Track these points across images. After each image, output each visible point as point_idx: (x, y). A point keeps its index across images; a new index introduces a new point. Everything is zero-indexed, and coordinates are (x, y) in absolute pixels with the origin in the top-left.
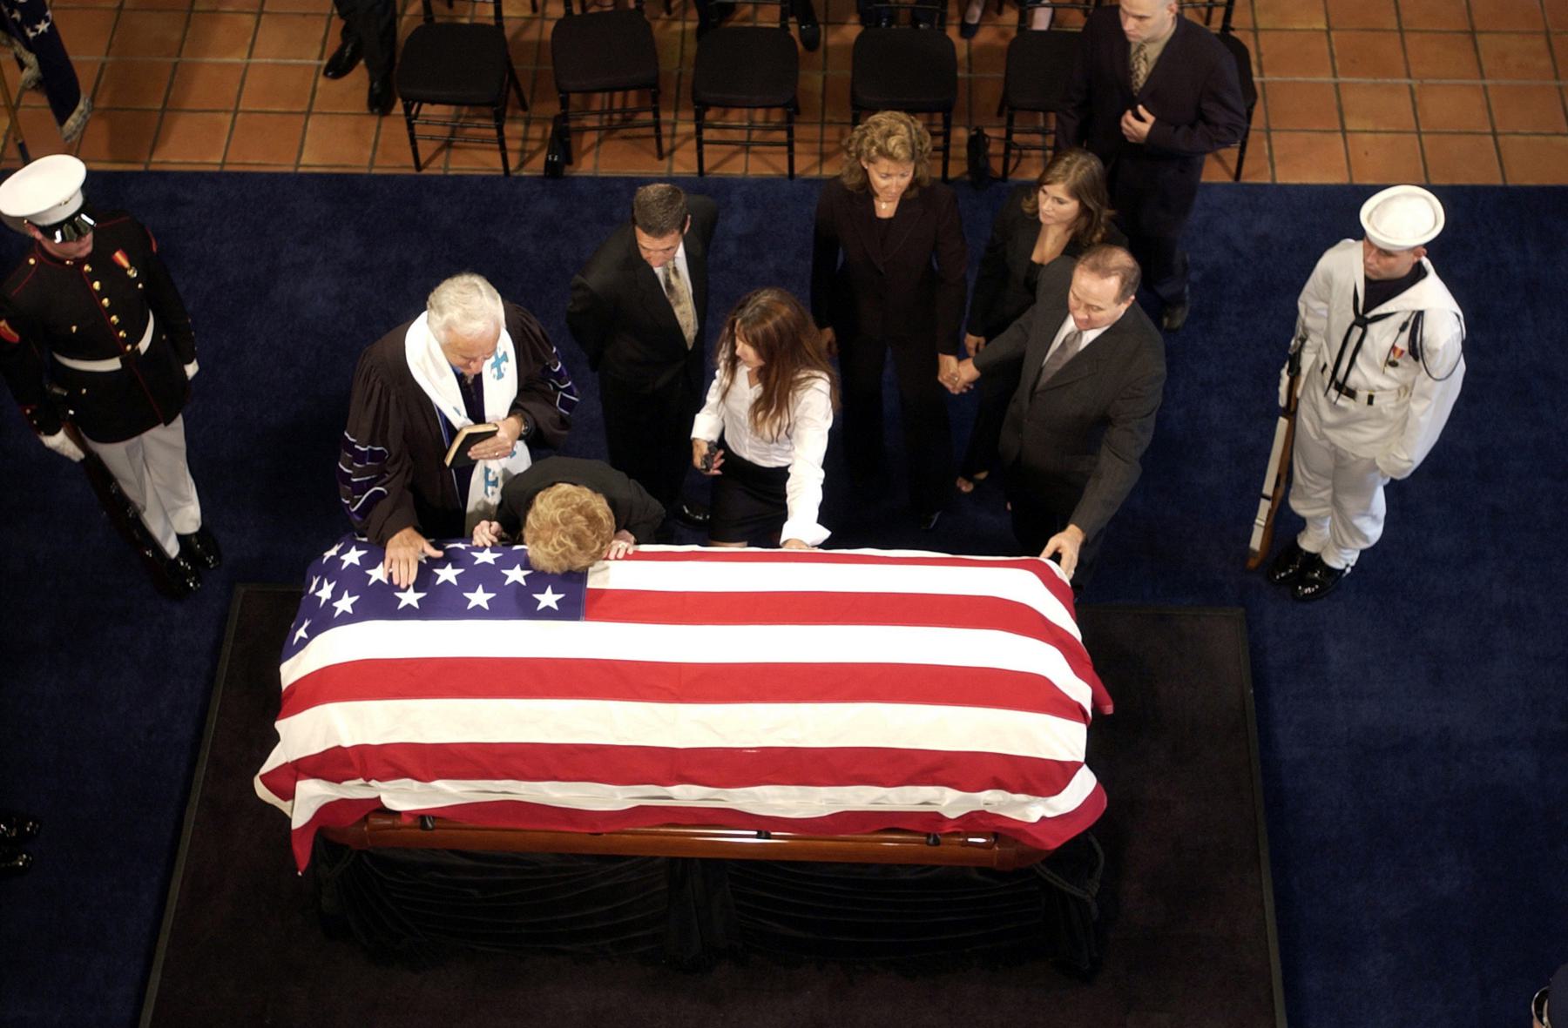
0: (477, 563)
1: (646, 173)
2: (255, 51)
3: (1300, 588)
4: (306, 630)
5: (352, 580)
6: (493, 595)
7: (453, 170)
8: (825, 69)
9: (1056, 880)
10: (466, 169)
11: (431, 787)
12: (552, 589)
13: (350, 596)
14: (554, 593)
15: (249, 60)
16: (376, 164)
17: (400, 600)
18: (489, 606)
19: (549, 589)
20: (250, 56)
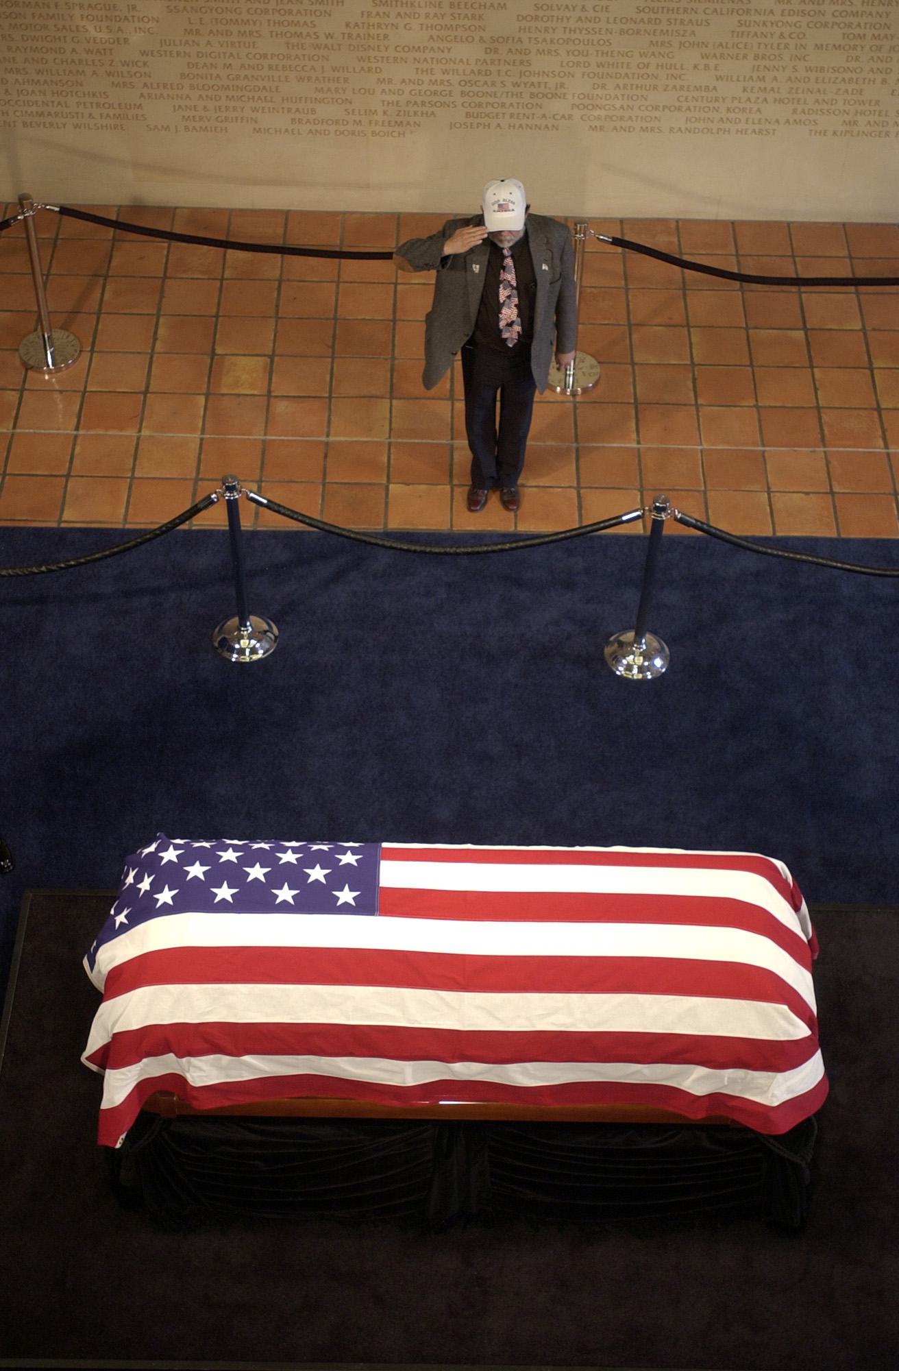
0: (281, 862)
1: (364, 529)
2: (18, 424)
3: (2, 863)
4: (126, 917)
5: (171, 875)
6: (358, 893)
7: (196, 525)
8: (138, 438)
9: (778, 1148)
10: (208, 525)
11: (449, 1068)
12: (288, 885)
13: (170, 890)
14: (229, 887)
15: (14, 431)
16: (128, 521)
17: (354, 898)
18: (233, 899)
19: (225, 884)
20: (14, 427)
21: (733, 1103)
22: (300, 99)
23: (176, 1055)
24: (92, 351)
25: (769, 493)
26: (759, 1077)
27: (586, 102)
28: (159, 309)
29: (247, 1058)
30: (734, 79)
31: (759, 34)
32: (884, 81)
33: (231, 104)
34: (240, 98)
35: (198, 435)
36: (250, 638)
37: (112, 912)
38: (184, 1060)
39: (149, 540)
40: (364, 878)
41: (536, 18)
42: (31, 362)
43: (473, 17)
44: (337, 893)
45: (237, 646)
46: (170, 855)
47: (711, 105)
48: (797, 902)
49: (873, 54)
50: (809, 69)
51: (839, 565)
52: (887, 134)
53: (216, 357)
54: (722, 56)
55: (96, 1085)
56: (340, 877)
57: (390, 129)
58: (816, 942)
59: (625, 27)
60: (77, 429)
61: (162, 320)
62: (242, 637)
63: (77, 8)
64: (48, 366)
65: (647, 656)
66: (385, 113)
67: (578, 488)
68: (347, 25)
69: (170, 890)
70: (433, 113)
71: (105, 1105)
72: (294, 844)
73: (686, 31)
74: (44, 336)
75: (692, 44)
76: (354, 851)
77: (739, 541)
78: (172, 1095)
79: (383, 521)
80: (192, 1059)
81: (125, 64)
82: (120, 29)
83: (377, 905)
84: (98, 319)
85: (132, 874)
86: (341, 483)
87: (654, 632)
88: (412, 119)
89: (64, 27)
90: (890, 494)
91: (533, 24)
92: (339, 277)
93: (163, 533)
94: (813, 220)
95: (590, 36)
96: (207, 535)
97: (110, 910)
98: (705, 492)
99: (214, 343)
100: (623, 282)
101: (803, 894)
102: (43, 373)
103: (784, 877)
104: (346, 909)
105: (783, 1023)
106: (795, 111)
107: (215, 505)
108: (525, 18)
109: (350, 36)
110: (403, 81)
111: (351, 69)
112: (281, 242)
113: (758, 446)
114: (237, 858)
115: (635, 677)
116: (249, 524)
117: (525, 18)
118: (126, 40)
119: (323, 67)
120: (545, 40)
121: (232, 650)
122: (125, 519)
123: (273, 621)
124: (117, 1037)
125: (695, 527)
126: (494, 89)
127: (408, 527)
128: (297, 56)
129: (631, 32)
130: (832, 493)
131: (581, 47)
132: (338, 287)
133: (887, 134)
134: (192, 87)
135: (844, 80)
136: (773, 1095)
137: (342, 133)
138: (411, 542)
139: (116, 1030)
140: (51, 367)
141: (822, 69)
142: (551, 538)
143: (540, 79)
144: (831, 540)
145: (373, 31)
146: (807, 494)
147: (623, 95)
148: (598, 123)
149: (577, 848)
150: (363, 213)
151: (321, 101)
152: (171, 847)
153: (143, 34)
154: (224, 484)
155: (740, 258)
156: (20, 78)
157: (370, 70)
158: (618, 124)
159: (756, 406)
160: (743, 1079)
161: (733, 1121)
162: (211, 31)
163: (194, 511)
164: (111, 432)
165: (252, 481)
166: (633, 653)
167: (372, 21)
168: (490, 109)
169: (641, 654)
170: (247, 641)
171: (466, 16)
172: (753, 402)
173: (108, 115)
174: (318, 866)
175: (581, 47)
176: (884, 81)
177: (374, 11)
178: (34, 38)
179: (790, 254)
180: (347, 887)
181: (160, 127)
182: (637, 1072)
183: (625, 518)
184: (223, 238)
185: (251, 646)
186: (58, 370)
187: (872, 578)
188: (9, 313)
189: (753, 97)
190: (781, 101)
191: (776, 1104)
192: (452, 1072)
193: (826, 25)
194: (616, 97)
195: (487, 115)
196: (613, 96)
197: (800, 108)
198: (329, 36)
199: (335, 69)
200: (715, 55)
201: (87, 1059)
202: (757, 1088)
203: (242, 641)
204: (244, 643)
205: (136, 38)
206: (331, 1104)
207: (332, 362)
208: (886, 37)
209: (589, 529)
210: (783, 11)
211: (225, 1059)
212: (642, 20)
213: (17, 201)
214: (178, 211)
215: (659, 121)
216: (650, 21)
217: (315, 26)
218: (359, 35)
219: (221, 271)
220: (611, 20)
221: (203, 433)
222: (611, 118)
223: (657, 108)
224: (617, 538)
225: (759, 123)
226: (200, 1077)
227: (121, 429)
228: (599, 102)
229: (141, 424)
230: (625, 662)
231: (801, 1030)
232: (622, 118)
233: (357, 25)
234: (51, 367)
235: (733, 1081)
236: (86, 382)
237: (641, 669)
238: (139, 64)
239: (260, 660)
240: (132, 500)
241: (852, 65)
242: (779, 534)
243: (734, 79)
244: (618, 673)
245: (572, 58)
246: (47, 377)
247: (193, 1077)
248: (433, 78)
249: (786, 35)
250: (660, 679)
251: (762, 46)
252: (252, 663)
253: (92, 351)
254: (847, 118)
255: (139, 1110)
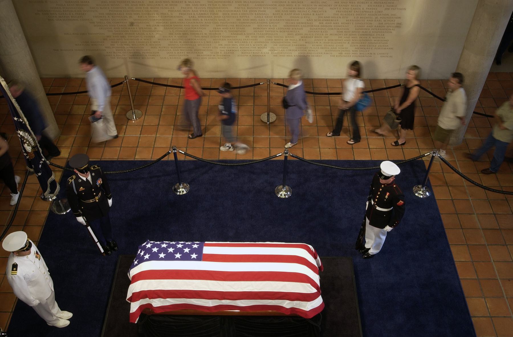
2: (125, 134)
4: (137, 262)
5: (148, 251)
8: (156, 137)
20: (124, 135)
21: (297, 310)
22: (199, 50)
23: (149, 298)
24: (145, 115)
25: (320, 148)
26: (304, 303)
27: (272, 49)
28: (163, 104)
29: (167, 299)
30: (310, 43)
31: (316, 31)
32: (348, 43)
33: (181, 52)
34: (184, 50)
35: (171, 136)
36: (182, 188)
37: (134, 261)
38: (151, 300)
39: (154, 163)
40: (199, 251)
41: (258, 28)
42: (129, 118)
43: (242, 28)
44: (191, 255)
45: (179, 191)
46: (149, 246)
47: (305, 49)
48: (316, 256)
49: (345, 36)
50: (329, 40)
51: (337, 167)
52: (350, 56)
53: (177, 116)
54: (306, 37)
55: (128, 306)
56: (192, 251)
57: (222, 57)
58: (322, 268)
59: (281, 30)
60: (140, 135)
61: (164, 106)
62: (180, 188)
63: (142, 29)
64: (134, 119)
65: (286, 191)
66: (221, 53)
67: (270, 148)
68: (210, 31)
69: (148, 254)
70: (233, 53)
71: (131, 312)
72: (182, 242)
73: (297, 31)
74: (133, 111)
75: (299, 34)
76: (197, 244)
77: (308, 161)
78: (150, 309)
79: (218, 157)
80: (153, 300)
81: (154, 42)
82: (152, 34)
83: (202, 258)
84: (147, 106)
85: (140, 251)
86: (208, 148)
87: (288, 185)
88: (228, 54)
89: (138, 34)
90: (351, 148)
91: (258, 30)
92: (210, 94)
93: (157, 161)
94: (333, 78)
95: (272, 33)
96: (168, 163)
97: (134, 260)
98: (303, 148)
99: (177, 112)
100: (283, 95)
101: (317, 254)
102: (133, 121)
103: (312, 250)
104: (194, 259)
105: (309, 289)
106: (326, 51)
107: (170, 154)
108: (255, 29)
109: (211, 34)
110: (225, 45)
111: (211, 42)
112: (210, 86)
113: (317, 136)
114: (198, 247)
115: (283, 197)
116: (183, 159)
117: (255, 29)
118: (154, 37)
119: (204, 42)
120: (261, 34)
121: (177, 192)
122: (151, 158)
123: (188, 184)
124: (133, 294)
125: (296, 157)
126: (248, 46)
127: (225, 159)
128: (198, 39)
129: (283, 31)
130: (336, 148)
131: (270, 35)
132: (209, 97)
133: (350, 56)
134: (171, 47)
135: (338, 43)
136: (307, 308)
137: (210, 58)
138: (225, 163)
139: (133, 292)
140: (135, 119)
141: (332, 40)
142: (258, 161)
143: (260, 44)
144: (335, 161)
145: (217, 33)
146: (329, 148)
147: (282, 47)
148: (276, 54)
149: (257, 243)
150: (217, 78)
151: (204, 50)
152: (149, 243)
153: (158, 35)
154: (172, 148)
155: (314, 88)
156: (128, 46)
157: (216, 42)
158: (281, 55)
159: (317, 126)
160: (299, 304)
161: (298, 315)
162: (176, 34)
163: (165, 156)
164: (149, 136)
165: (185, 147)
166: (282, 191)
167: (216, 30)
168: (248, 51)
169: (284, 191)
170: (181, 189)
171: (240, 28)
172: (316, 125)
173: (150, 55)
174: (187, 248)
175: (270, 35)
176: (348, 43)
177: (217, 28)
178: (131, 37)
179: (327, 87)
180: (178, 253)
181: (164, 58)
182: (271, 302)
183: (277, 155)
184: (180, 86)
185: (182, 190)
186: (136, 120)
187: (346, 170)
188: (124, 106)
189: (315, 47)
190: (322, 48)
191: (308, 310)
192: (222, 303)
193: (332, 29)
194: (280, 48)
195: (247, 53)
196: (279, 47)
197: (327, 50)
198: (205, 34)
199: (207, 42)
200: (305, 37)
201: (128, 299)
202: (303, 306)
203: (180, 189)
204: (181, 190)
205: (157, 36)
206: (191, 311)
207: (207, 116)
208: (348, 32)
209: (268, 158)
210: (321, 26)
211: (162, 300)
212: (285, 28)
213: (124, 77)
214: (169, 79)
215: (291, 53)
216: (287, 29)
217: (202, 32)
218: (213, 34)
219: (179, 93)
220: (277, 29)
221: (172, 135)
222: (279, 53)
223: (291, 50)
224: (275, 161)
225: (317, 53)
226: (156, 304)
227: (151, 135)
228: (275, 49)
229: (157, 133)
230: (280, 193)
231: (314, 290)
232: (282, 53)
233: (212, 31)
234: (135, 119)
235: (296, 304)
236: (143, 123)
237: (285, 195)
238: (158, 42)
239: (185, 194)
240: (153, 153)
241: (340, 39)
242: (322, 159)
243: (310, 43)
244: (279, 196)
245: (268, 38)
246: (133, 122)
247: (154, 304)
248: (233, 44)
249: (323, 31)
250: (289, 197)
251: (317, 34)
252: (183, 195)
253: (145, 115)
254: (340, 52)
255: (140, 313)
